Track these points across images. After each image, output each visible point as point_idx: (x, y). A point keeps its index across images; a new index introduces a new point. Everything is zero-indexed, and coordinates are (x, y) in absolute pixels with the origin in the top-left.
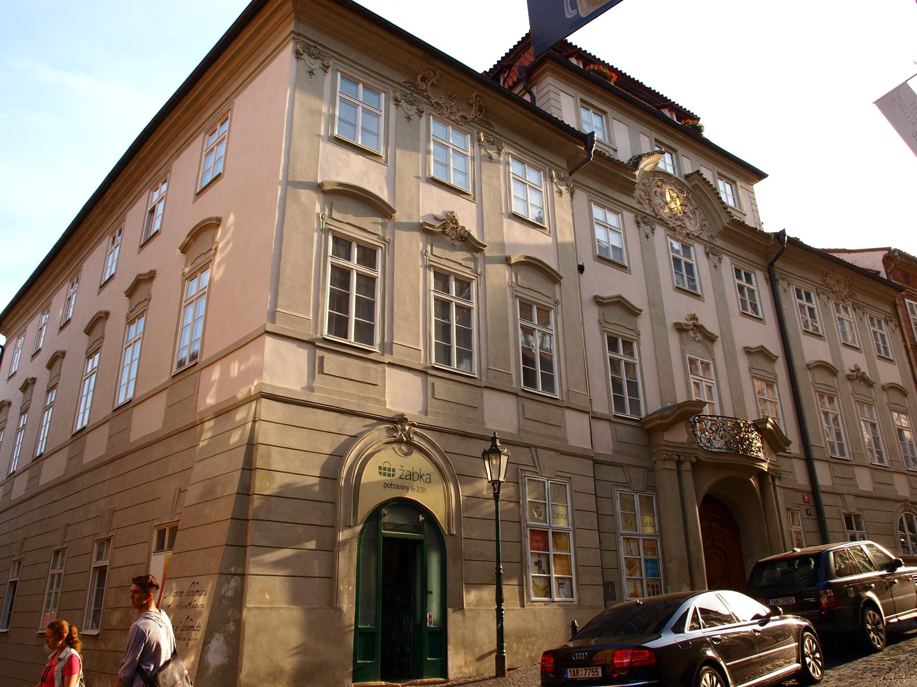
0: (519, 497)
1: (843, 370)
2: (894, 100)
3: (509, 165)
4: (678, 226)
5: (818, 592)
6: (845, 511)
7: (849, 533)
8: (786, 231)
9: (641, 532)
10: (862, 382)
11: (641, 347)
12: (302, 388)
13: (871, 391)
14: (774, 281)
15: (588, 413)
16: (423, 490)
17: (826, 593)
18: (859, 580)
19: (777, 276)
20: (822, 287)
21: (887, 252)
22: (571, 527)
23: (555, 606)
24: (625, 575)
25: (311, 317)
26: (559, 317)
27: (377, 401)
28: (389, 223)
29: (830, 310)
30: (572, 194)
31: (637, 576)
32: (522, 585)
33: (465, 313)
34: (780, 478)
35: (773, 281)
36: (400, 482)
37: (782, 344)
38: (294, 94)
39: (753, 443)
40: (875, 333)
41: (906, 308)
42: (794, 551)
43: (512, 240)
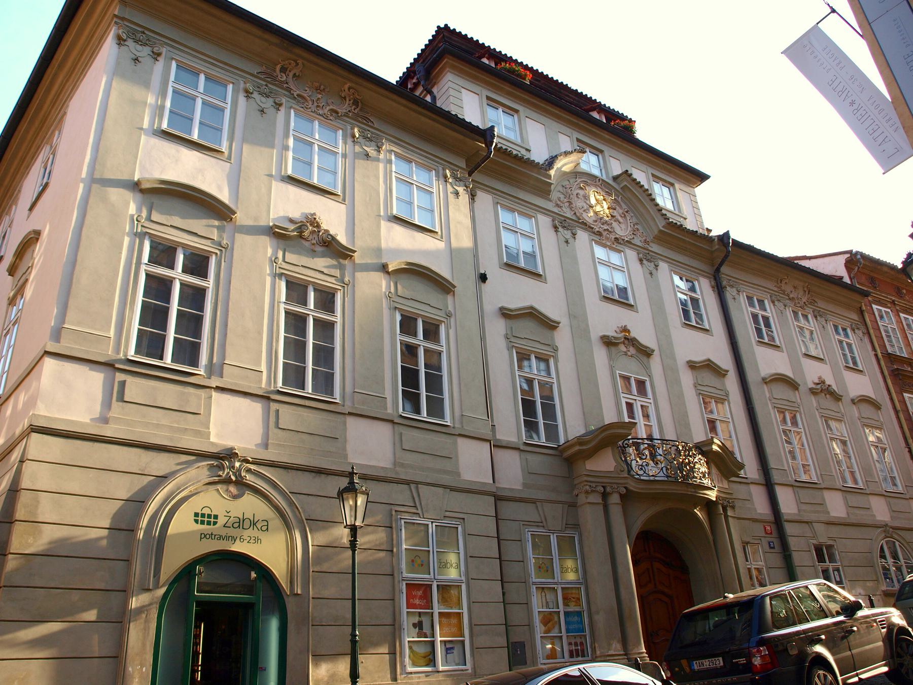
0: (392, 544)
1: (806, 383)
2: (805, 46)
3: (392, 164)
4: (605, 230)
5: (749, 651)
6: (815, 542)
7: (820, 567)
8: (730, 233)
9: (559, 579)
10: (828, 396)
11: (559, 364)
12: (92, 420)
13: (839, 406)
14: (722, 288)
15: (490, 441)
16: (257, 540)
17: (759, 651)
18: (805, 631)
19: (724, 283)
20: (777, 294)
21: (848, 255)
22: (463, 578)
23: (440, 677)
24: (539, 633)
25: (112, 333)
26: (452, 332)
27: (198, 433)
28: (228, 226)
29: (787, 318)
30: (473, 196)
31: (555, 633)
32: (395, 654)
33: (325, 328)
34: (733, 507)
35: (720, 289)
36: (224, 532)
37: (733, 358)
38: (112, 82)
39: (695, 468)
40: (841, 342)
41: (874, 314)
42: (725, 597)
43: (392, 245)
